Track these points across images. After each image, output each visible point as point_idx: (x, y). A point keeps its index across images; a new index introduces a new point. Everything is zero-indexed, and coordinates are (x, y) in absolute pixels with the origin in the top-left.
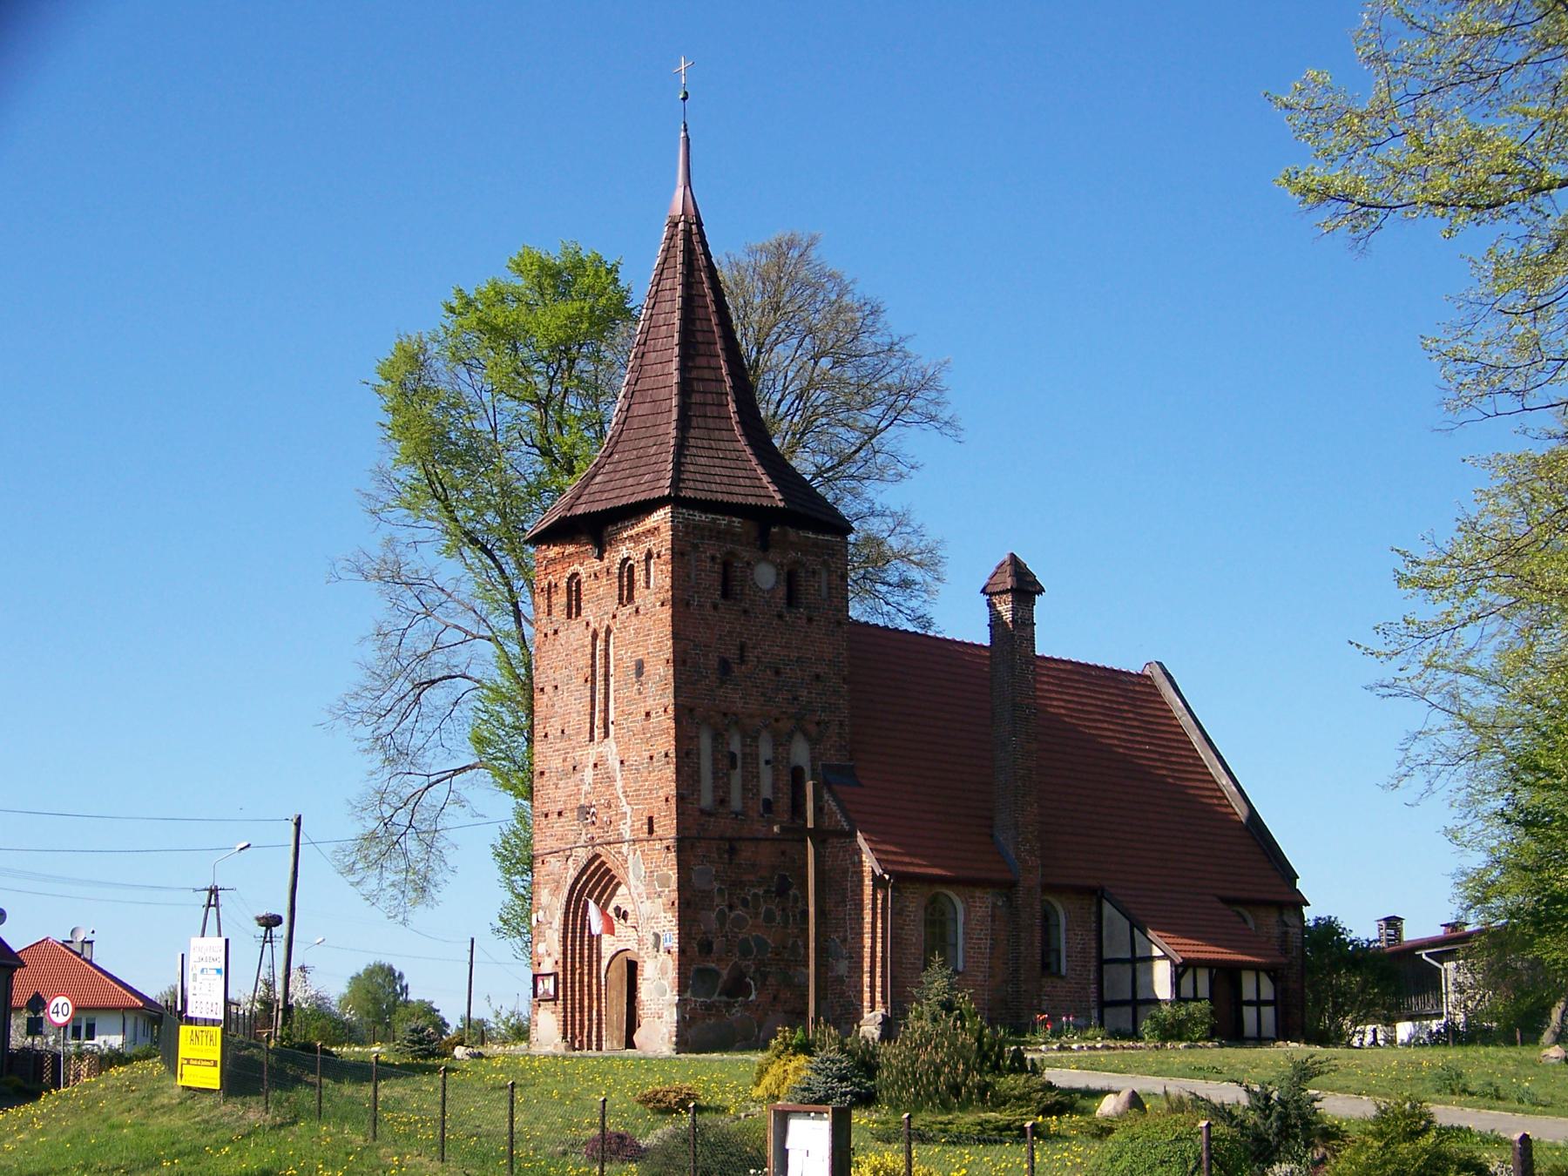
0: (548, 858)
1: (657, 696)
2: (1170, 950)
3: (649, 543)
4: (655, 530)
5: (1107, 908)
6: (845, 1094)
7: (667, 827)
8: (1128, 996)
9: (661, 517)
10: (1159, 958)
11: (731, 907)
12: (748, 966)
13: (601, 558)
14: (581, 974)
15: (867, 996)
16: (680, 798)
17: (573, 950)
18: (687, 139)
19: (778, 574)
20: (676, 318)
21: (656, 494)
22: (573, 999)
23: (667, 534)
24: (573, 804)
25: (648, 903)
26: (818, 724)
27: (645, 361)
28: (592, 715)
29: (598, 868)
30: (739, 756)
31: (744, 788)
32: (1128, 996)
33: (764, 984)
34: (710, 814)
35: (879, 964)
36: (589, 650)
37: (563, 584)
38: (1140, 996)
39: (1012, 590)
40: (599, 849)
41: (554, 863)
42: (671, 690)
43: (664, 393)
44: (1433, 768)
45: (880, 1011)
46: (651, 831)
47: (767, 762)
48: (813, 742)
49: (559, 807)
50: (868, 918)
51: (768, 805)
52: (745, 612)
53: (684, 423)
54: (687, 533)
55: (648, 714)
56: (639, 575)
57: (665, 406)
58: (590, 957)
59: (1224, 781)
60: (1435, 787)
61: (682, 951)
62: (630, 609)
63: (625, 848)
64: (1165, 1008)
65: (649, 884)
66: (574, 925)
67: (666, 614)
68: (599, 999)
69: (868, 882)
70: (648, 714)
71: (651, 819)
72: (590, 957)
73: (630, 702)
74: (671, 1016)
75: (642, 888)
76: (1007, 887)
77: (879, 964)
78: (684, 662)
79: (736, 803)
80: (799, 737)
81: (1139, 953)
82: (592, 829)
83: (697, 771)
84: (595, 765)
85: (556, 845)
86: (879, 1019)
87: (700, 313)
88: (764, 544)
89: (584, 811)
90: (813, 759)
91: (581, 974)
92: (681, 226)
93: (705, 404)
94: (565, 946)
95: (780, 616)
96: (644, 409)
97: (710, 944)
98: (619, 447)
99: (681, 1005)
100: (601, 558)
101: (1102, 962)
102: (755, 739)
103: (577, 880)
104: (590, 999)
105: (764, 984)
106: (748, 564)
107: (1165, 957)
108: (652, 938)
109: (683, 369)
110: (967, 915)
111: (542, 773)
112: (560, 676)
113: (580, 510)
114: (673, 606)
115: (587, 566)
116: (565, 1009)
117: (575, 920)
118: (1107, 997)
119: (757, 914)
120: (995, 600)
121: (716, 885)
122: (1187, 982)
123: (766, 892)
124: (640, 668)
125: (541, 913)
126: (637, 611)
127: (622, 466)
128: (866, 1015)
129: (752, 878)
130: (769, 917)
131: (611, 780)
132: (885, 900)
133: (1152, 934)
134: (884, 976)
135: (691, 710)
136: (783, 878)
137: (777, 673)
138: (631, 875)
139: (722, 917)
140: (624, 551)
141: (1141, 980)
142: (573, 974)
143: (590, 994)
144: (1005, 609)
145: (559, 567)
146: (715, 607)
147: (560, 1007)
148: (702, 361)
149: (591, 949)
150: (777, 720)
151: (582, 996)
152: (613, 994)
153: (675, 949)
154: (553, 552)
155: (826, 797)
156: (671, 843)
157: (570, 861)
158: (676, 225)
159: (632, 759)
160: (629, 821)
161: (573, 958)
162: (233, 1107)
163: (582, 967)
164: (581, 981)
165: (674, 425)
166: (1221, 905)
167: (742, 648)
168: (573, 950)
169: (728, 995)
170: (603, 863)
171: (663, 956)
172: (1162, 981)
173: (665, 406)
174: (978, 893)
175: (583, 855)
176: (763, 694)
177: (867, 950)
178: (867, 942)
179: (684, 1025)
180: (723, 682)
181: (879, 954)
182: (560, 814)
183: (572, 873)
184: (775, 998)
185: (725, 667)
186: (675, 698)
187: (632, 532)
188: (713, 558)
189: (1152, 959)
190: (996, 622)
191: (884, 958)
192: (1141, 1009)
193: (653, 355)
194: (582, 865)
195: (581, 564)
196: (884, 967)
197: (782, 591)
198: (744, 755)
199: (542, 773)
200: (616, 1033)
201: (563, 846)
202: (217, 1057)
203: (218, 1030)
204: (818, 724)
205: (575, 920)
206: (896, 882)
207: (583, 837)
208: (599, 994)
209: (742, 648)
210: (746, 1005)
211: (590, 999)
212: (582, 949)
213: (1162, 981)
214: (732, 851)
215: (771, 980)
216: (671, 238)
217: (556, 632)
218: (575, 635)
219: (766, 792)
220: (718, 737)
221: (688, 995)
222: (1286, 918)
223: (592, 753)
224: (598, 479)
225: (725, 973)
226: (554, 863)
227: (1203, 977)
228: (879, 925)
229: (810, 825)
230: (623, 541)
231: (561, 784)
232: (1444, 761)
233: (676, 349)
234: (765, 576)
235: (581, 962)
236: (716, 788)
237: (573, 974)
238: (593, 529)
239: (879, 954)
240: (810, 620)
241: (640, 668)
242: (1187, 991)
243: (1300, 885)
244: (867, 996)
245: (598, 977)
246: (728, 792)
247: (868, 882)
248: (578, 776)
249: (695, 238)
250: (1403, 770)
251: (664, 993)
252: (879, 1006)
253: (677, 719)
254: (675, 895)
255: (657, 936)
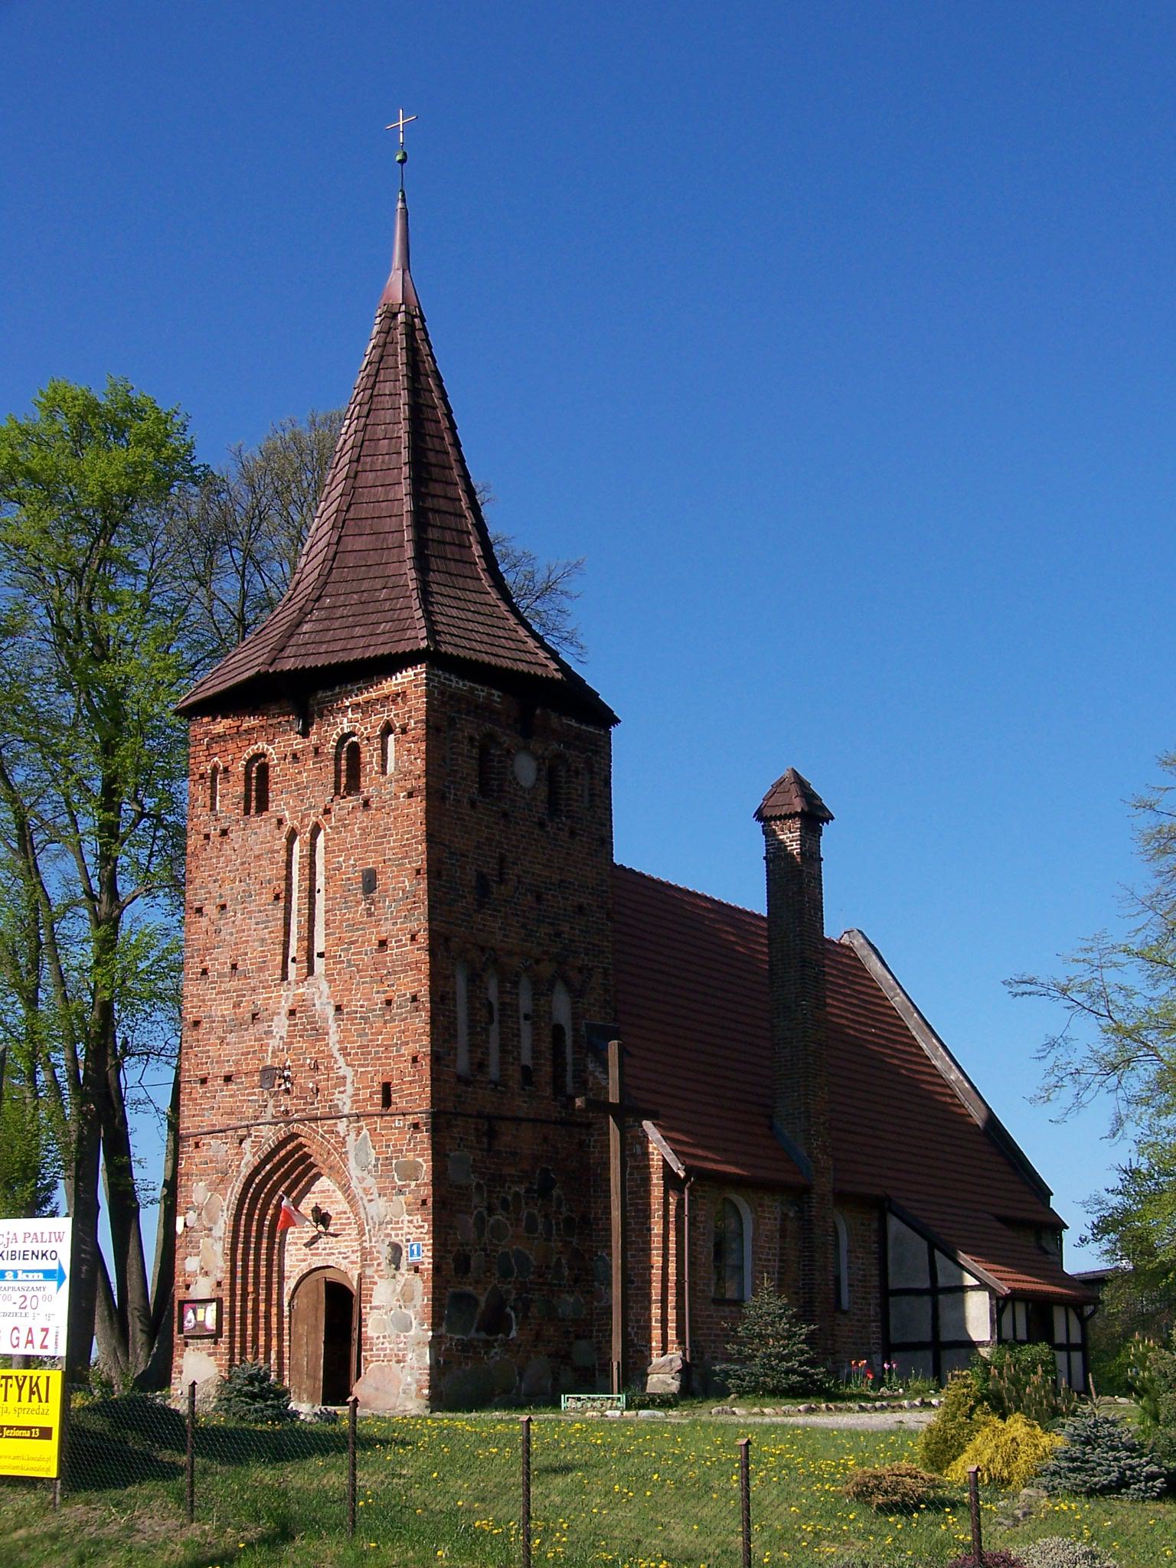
0: (206, 1139)
1: (403, 917)
2: (991, 1278)
3: (391, 713)
4: (401, 695)
5: (894, 1225)
6: (1152, 1477)
7: (416, 1094)
8: (927, 1336)
9: (410, 678)
10: (973, 1288)
11: (491, 1210)
12: (508, 1292)
13: (305, 734)
14: (256, 1301)
15: (656, 1333)
16: (436, 1058)
17: (245, 1267)
18: (405, 208)
19: (539, 770)
20: (403, 430)
21: (404, 647)
22: (243, 1336)
23: (418, 702)
24: (253, 1064)
25: (382, 1201)
26: (580, 970)
27: (359, 483)
28: (286, 945)
29: (291, 1154)
30: (496, 1006)
31: (503, 1050)
32: (927, 1336)
33: (526, 1316)
34: (468, 1083)
35: (672, 1291)
36: (282, 856)
37: (239, 768)
38: (946, 1336)
39: (801, 815)
40: (296, 1128)
41: (217, 1148)
42: (423, 909)
43: (389, 524)
44: (1083, 1078)
45: (675, 1355)
46: (387, 1101)
47: (526, 1017)
48: (577, 994)
49: (226, 1069)
50: (657, 1229)
51: (527, 1074)
52: (505, 815)
53: (422, 563)
54: (443, 704)
55: (383, 943)
56: (369, 755)
57: (392, 540)
58: (269, 1277)
59: (954, 1076)
60: (1084, 1100)
61: (437, 1269)
62: (351, 802)
63: (342, 1126)
64: (984, 1352)
65: (385, 1174)
66: (248, 1231)
67: (417, 808)
68: (280, 1336)
69: (657, 1179)
70: (383, 943)
71: (386, 1088)
72: (269, 1277)
73: (353, 927)
74: (419, 1360)
75: (370, 1181)
76: (798, 1194)
77: (672, 1291)
78: (439, 875)
79: (494, 1071)
80: (560, 987)
81: (942, 1282)
82: (286, 1102)
83: (453, 1023)
84: (292, 1013)
85: (219, 1121)
86: (678, 1364)
87: (430, 428)
88: (527, 729)
89: (269, 1075)
90: (576, 1016)
91: (256, 1301)
92: (401, 317)
93: (444, 543)
94: (233, 1261)
95: (541, 825)
96: (359, 543)
97: (467, 1258)
98: (329, 589)
99: (435, 1344)
100: (305, 734)
101: (886, 1293)
102: (516, 984)
103: (256, 1171)
104: (268, 1336)
105: (526, 1316)
106: (509, 751)
107: (983, 1286)
108: (386, 1251)
109: (417, 495)
110: (756, 1228)
111: (197, 1023)
112: (230, 891)
113: (289, 665)
114: (429, 797)
115: (279, 744)
116: (232, 1349)
117: (248, 1225)
118: (895, 1338)
119: (519, 1220)
120: (776, 826)
121: (474, 1180)
122: (1007, 1318)
123: (527, 1191)
124: (370, 881)
125: (192, 1216)
126: (366, 804)
127: (339, 612)
128: (656, 1360)
129: (513, 1171)
130: (531, 1227)
131: (319, 1033)
132: (680, 1206)
133: (964, 1258)
134: (679, 1308)
135: (447, 939)
136: (545, 1171)
137: (539, 898)
138: (352, 1163)
139: (481, 1221)
140: (345, 724)
141: (946, 1316)
142: (244, 1301)
143: (268, 1329)
144: (790, 837)
145: (231, 746)
146: (473, 804)
147: (223, 1347)
148: (437, 488)
149: (269, 1266)
150: (538, 961)
151: (256, 1329)
152: (302, 1329)
153: (427, 1264)
154: (221, 726)
155: (591, 1066)
156: (422, 1118)
157: (247, 1144)
158: (395, 315)
159: (356, 1003)
160: (350, 1089)
161: (245, 1278)
162: (75, 1512)
163: (256, 1291)
164: (256, 1310)
165: (409, 564)
166: (998, 1225)
167: (502, 860)
168: (245, 1267)
169: (489, 1333)
170: (301, 1146)
171: (405, 1275)
172: (977, 1316)
173: (392, 540)
174: (767, 1201)
175: (269, 1135)
176: (524, 926)
177: (656, 1272)
178: (657, 1260)
179: (438, 1371)
180: (481, 905)
181: (672, 1278)
182: (228, 1079)
183: (249, 1158)
184: (538, 1336)
185: (483, 885)
186: (430, 921)
187: (360, 699)
188: (471, 739)
189: (963, 1289)
190: (776, 854)
191: (679, 1284)
192: (946, 1355)
193: (371, 475)
194: (266, 1149)
195: (270, 742)
196: (680, 1295)
197: (543, 793)
198: (503, 1004)
199: (197, 1023)
200: (307, 1383)
201: (234, 1123)
202: (52, 1418)
203: (56, 1377)
204: (580, 970)
205: (248, 1225)
206: (695, 1184)
207: (270, 1110)
208: (280, 1329)
209: (502, 860)
210: (506, 1345)
211: (268, 1336)
212: (257, 1266)
213: (977, 1316)
214: (492, 1134)
215: (534, 1311)
216: (387, 331)
217: (224, 833)
218: (261, 834)
219: (526, 1059)
220: (475, 979)
221: (443, 1330)
222: (1044, 1244)
223: (285, 997)
224: (306, 628)
225: (482, 1300)
226: (217, 1148)
227: (1021, 1310)
228: (672, 1238)
229: (614, 1098)
230: (343, 711)
231: (231, 1038)
232: (1095, 1070)
233: (406, 470)
234: (526, 769)
235: (256, 1284)
236: (472, 1048)
237: (244, 1301)
238: (294, 693)
239: (672, 1278)
240: (573, 834)
241: (370, 881)
242: (1007, 1333)
243: (1054, 1203)
244: (656, 1333)
245: (280, 1306)
246: (486, 1054)
247: (657, 1179)
248: (262, 1027)
249: (419, 335)
250: (1053, 1080)
251: (408, 1328)
252: (673, 1347)
253: (432, 951)
254: (427, 1191)
255: (396, 1249)
